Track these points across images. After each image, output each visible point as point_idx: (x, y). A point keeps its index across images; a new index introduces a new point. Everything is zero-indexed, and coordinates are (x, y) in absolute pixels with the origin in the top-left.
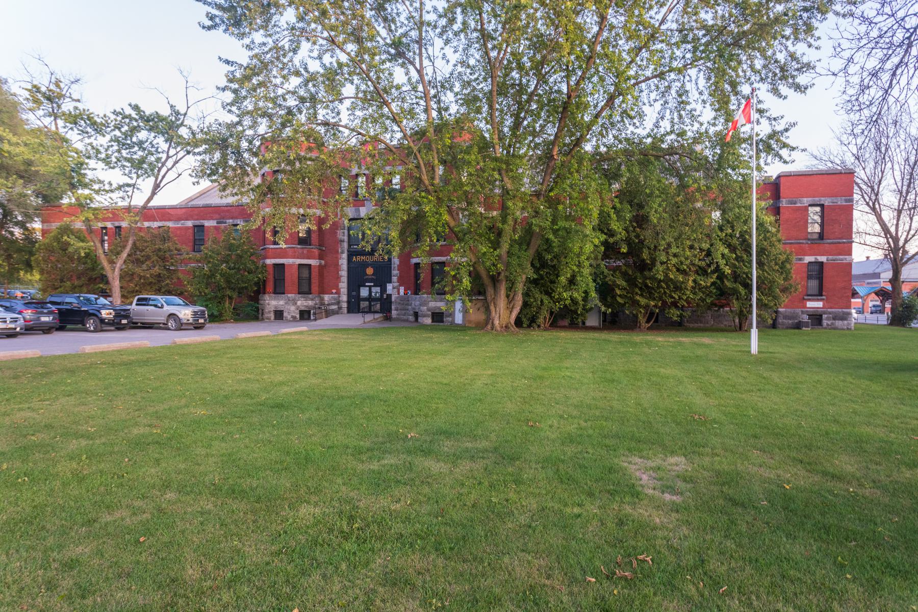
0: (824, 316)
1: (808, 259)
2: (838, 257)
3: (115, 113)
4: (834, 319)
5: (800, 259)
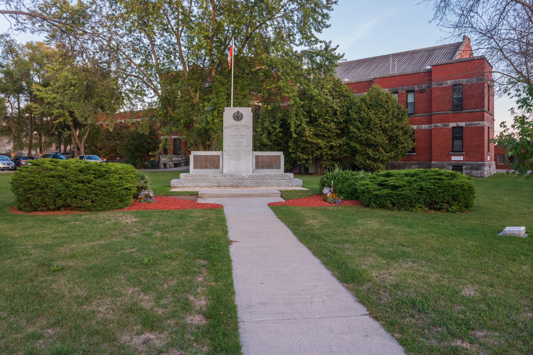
0: (464, 167)
1: (452, 125)
2: (473, 123)
3: (517, 103)
4: (471, 169)
5: (446, 125)
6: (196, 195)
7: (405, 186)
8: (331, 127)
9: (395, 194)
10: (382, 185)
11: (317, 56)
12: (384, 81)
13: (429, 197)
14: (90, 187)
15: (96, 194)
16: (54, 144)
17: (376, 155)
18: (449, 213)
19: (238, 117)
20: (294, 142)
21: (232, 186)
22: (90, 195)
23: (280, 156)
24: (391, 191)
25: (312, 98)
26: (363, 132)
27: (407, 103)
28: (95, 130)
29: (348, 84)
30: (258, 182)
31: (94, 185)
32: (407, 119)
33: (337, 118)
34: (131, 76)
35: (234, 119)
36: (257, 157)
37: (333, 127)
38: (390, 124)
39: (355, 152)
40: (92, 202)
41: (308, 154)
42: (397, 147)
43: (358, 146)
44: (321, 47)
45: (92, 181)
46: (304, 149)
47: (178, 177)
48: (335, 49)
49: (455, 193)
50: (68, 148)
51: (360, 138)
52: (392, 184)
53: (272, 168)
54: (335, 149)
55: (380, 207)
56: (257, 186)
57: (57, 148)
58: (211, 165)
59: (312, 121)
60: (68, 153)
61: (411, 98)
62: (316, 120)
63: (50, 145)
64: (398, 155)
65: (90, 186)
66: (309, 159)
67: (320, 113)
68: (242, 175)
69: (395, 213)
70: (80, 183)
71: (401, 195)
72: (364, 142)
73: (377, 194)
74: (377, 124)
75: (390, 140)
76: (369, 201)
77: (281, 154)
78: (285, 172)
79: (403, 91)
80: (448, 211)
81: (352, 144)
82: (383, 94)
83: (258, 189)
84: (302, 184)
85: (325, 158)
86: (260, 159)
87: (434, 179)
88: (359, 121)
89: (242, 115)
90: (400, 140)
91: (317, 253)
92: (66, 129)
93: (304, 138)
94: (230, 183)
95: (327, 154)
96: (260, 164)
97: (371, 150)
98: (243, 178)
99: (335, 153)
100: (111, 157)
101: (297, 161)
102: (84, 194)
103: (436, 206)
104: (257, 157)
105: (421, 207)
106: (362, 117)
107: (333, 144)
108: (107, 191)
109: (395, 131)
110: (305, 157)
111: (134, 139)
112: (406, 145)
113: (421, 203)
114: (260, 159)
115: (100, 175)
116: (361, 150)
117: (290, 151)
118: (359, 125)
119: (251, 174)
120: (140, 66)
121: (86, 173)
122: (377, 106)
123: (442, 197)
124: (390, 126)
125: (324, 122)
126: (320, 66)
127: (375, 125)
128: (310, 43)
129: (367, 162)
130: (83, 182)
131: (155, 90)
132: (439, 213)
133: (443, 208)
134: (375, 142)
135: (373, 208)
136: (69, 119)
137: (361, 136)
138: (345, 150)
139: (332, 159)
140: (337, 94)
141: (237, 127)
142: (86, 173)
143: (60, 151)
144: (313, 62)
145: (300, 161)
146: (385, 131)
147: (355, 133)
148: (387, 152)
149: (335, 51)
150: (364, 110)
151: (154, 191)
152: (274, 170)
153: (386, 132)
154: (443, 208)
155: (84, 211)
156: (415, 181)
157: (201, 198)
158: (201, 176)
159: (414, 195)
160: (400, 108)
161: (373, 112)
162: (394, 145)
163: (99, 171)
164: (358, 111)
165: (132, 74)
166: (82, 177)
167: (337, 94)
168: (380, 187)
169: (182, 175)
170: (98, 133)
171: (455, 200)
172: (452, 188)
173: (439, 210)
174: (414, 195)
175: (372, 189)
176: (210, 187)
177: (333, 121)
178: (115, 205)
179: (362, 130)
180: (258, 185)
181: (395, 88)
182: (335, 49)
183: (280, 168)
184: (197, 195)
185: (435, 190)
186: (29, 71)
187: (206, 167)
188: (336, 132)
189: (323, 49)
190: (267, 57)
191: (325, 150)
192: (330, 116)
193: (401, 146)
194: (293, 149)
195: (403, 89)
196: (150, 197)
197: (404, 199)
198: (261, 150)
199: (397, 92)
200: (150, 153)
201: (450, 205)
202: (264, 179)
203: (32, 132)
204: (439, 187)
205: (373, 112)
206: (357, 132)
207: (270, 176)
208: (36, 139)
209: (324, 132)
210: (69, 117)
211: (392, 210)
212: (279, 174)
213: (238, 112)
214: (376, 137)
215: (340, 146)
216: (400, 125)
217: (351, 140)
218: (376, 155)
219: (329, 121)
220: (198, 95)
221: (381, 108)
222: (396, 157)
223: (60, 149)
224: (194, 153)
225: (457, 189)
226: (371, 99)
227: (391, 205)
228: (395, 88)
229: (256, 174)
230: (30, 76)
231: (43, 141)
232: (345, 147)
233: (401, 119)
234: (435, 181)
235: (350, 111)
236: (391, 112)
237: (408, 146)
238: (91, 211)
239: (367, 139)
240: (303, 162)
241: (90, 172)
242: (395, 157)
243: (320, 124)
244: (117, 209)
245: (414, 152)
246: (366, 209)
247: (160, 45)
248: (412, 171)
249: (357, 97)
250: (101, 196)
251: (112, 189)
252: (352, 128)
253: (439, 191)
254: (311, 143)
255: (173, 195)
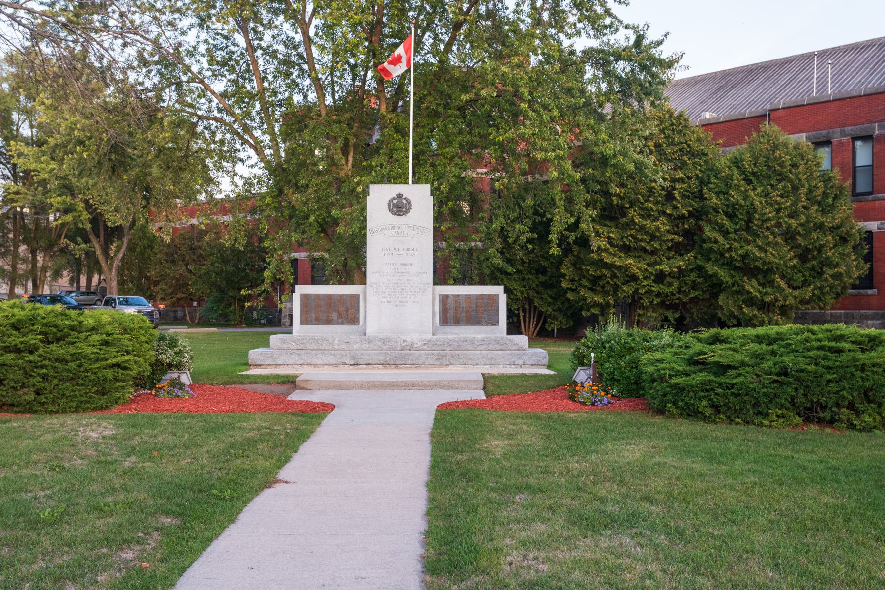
6: (291, 382)
7: (743, 364)
8: (658, 229)
9: (720, 385)
10: (697, 363)
11: (616, 61)
12: (793, 115)
13: (801, 392)
14: (31, 362)
15: (44, 377)
16: (65, 273)
17: (766, 293)
18: (853, 433)
19: (400, 207)
20: (574, 265)
21: (385, 364)
22: (31, 379)
23: (497, 296)
24: (712, 377)
25: (604, 161)
26: (735, 240)
27: (855, 168)
28: (145, 242)
29: (707, 125)
30: (443, 355)
31: (40, 356)
32: (846, 207)
33: (675, 208)
34: (208, 118)
35: (391, 211)
36: (444, 299)
37: (663, 228)
38: (803, 218)
39: (716, 287)
40: (38, 393)
41: (606, 293)
42: (821, 274)
43: (723, 274)
44: (627, 39)
45: (37, 349)
46: (595, 280)
47: (267, 344)
48: (659, 43)
49: (868, 384)
50: (95, 279)
51: (727, 255)
52: (716, 359)
53: (478, 323)
54: (668, 279)
55: (689, 415)
56: (441, 365)
57: (72, 280)
58: (340, 316)
59: (611, 214)
60: (94, 293)
61: (863, 155)
62: (622, 211)
63: (57, 274)
64: (823, 294)
65: (31, 358)
66: (608, 304)
67: (633, 196)
68: (409, 339)
69: (721, 430)
70: (10, 352)
71: (733, 385)
72: (737, 264)
73: (678, 384)
74: (769, 219)
75: (804, 256)
76: (662, 401)
77: (498, 290)
78: (508, 333)
79: (844, 139)
80: (852, 426)
81: (710, 268)
82: (785, 145)
83: (442, 370)
84: (546, 361)
85: (646, 302)
86: (450, 300)
87: (819, 348)
88: (726, 213)
89: (408, 201)
90: (828, 258)
91: (437, 511)
92: (79, 239)
93: (595, 256)
94: (382, 358)
95: (649, 292)
96: (451, 314)
97: (754, 282)
98: (411, 347)
99: (668, 290)
100: (178, 299)
101: (581, 309)
102: (19, 375)
103: (821, 415)
104: (444, 299)
105: (783, 416)
106: (733, 205)
107: (665, 267)
108: (69, 371)
109: (814, 235)
110: (598, 299)
111: (225, 261)
112: (842, 269)
113: (782, 407)
114: (451, 303)
115: (59, 334)
116: (730, 281)
117: (565, 285)
118: (727, 223)
119: (429, 336)
120: (224, 95)
121: (26, 330)
122: (769, 177)
123: (837, 393)
124: (801, 225)
125: (642, 217)
126: (627, 84)
127: (764, 221)
128: (599, 31)
129: (746, 310)
130: (18, 350)
131: (258, 148)
132: (828, 430)
133: (840, 420)
134: (764, 263)
135: (672, 417)
136: (85, 216)
137: (730, 249)
138: (694, 282)
139: (662, 304)
140: (676, 149)
141: (399, 226)
142: (26, 330)
143: (78, 287)
144: (609, 75)
145: (588, 310)
146: (789, 236)
147: (716, 242)
148: (795, 288)
149: (661, 48)
150: (738, 186)
151: (194, 376)
152: (484, 328)
153: (793, 238)
154: (840, 420)
155: (19, 412)
156: (774, 353)
157: (303, 389)
158: (316, 341)
159: (764, 387)
160: (830, 179)
161: (759, 190)
162: (813, 269)
163: (55, 326)
164: (723, 188)
165: (211, 114)
166: (16, 339)
167: (676, 149)
168: (692, 368)
169: (274, 339)
170: (151, 247)
171: (870, 402)
172: (863, 370)
173: (831, 422)
174: (764, 387)
175: (668, 372)
176: (336, 365)
177: (664, 213)
178: (86, 402)
179: (732, 236)
180: (445, 363)
181: (824, 132)
182: (659, 43)
183: (495, 323)
184: (294, 382)
185: (818, 376)
186: (10, 115)
187: (329, 322)
188: (672, 240)
189: (632, 43)
190: (494, 70)
191: (645, 283)
192: (657, 203)
193: (830, 272)
194: (573, 280)
195: (843, 134)
196: (182, 386)
197: (740, 395)
198: (464, 279)
199: (827, 142)
200: (243, 292)
201: (858, 413)
202: (459, 348)
203: (16, 247)
204: (829, 368)
205: (759, 190)
206: (721, 239)
207: (472, 342)
208: (25, 261)
209: (641, 241)
210: (85, 213)
211: (714, 422)
212: (492, 336)
213: (400, 196)
214: (766, 251)
215: (681, 273)
216: (828, 221)
217: (709, 259)
218: (766, 293)
219: (656, 214)
220: (350, 159)
221: (780, 181)
222: (819, 299)
223: (78, 283)
224: (302, 289)
225: (874, 373)
226: (756, 159)
227: (709, 411)
228: (824, 132)
229: (441, 337)
230: (12, 123)
231: (39, 265)
232: (693, 276)
233: (833, 207)
234: (821, 353)
235: (705, 191)
236: (803, 191)
237: (848, 273)
238: (36, 412)
239: (744, 257)
240: (593, 310)
241: (35, 328)
242: (816, 299)
243: (633, 221)
244: (94, 409)
245: (871, 288)
246: (659, 420)
247: (268, 47)
248: (772, 330)
249: (723, 155)
250: (56, 381)
251: (80, 366)
252: (708, 231)
253: (829, 377)
254: (610, 266)
255: (242, 383)
